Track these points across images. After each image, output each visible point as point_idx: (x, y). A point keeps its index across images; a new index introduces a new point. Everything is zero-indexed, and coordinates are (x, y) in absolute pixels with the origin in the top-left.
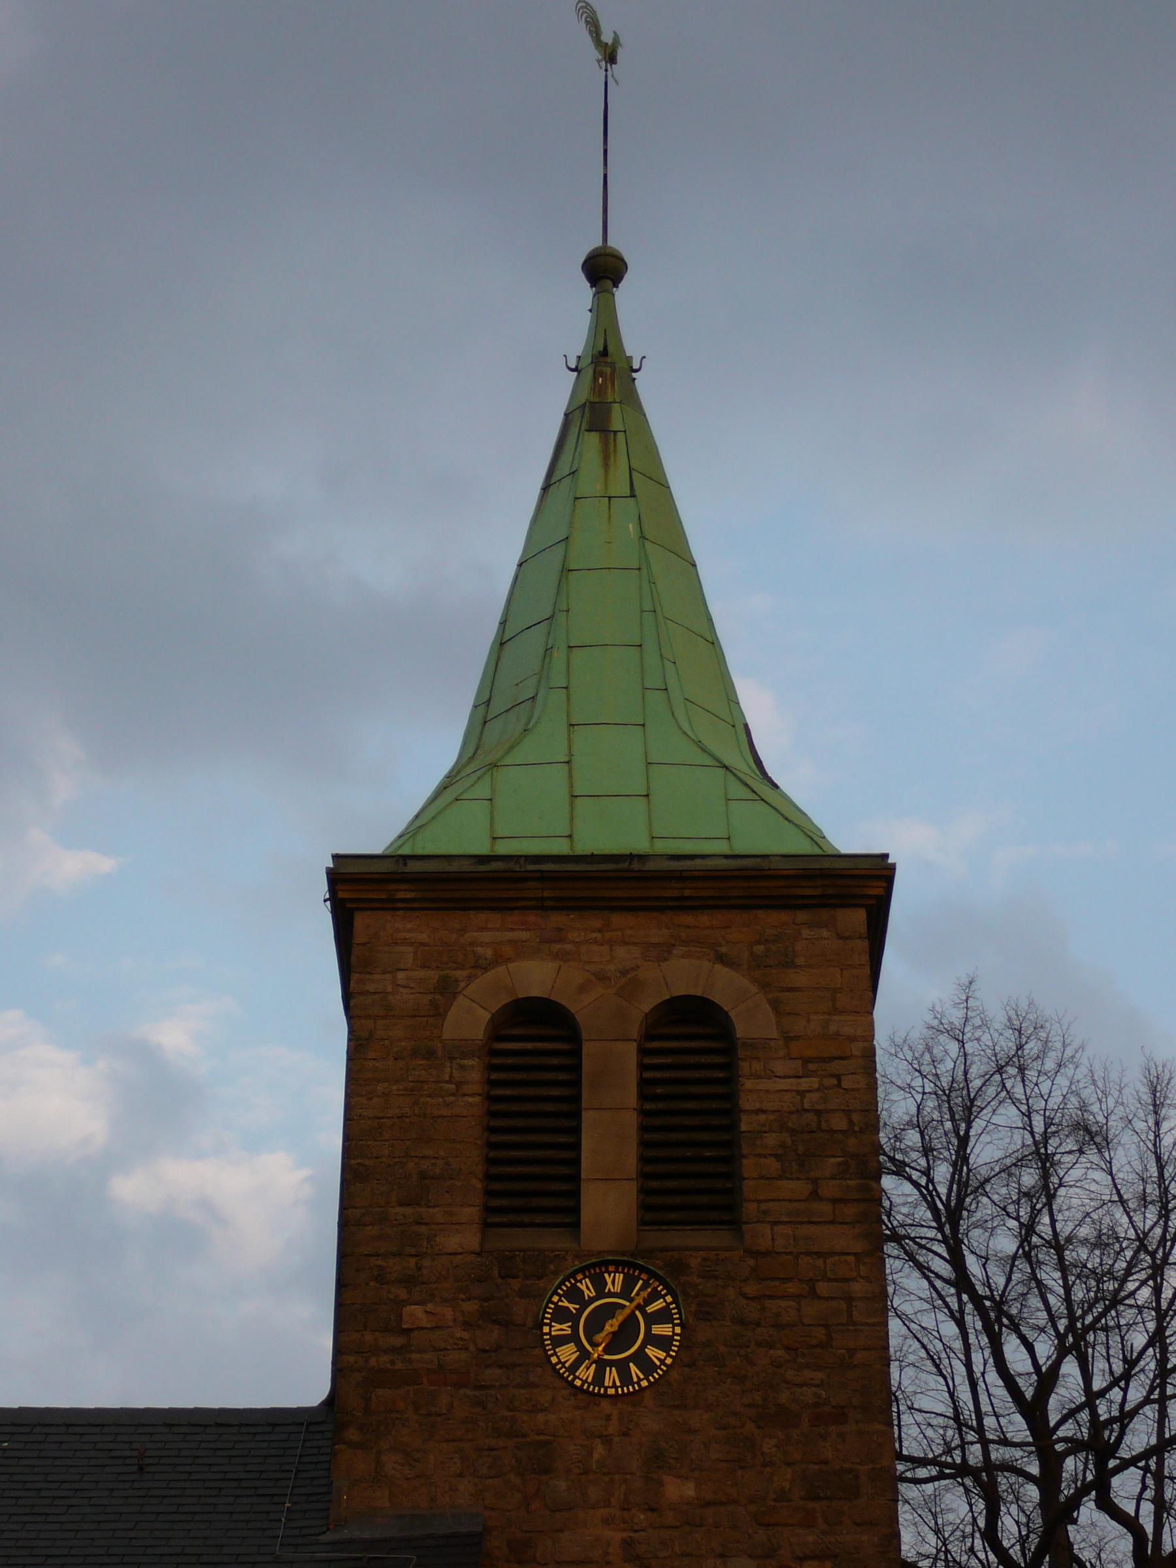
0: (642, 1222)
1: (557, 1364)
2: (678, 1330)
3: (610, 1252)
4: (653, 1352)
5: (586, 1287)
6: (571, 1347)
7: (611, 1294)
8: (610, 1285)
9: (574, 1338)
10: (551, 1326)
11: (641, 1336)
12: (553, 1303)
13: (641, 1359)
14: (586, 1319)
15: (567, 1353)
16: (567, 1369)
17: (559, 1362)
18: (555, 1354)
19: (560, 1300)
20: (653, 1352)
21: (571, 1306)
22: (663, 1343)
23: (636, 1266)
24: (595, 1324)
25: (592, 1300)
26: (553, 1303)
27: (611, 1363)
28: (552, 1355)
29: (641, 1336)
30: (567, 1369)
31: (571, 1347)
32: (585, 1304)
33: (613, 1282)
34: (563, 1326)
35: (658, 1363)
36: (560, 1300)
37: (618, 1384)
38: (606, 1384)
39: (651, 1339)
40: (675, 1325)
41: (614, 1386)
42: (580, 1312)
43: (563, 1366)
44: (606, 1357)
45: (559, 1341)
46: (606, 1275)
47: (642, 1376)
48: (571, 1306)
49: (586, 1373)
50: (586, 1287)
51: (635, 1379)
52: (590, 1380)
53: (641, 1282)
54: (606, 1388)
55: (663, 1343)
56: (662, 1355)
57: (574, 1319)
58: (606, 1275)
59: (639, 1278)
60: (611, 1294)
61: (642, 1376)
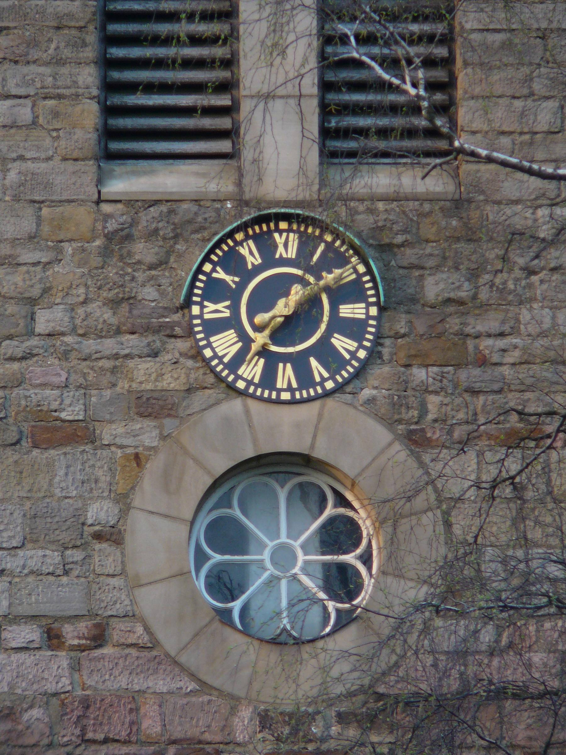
0: (328, 156)
1: (212, 358)
2: (374, 311)
3: (286, 204)
4: (342, 343)
5: (250, 254)
6: (230, 335)
7: (284, 262)
8: (281, 249)
9: (233, 322)
10: (202, 307)
11: (326, 319)
12: (204, 273)
13: (324, 352)
14: (293, 345)
15: (225, 344)
16: (226, 366)
17: (215, 356)
18: (209, 345)
19: (324, 380)
20: (342, 343)
21: (228, 278)
22: (354, 328)
23: (313, 222)
24: (264, 299)
25: (258, 270)
26: (204, 273)
27: (285, 358)
28: (205, 347)
29: (326, 319)
30: (226, 366)
31: (230, 335)
32: (247, 275)
33: (286, 245)
34: (220, 306)
35: (347, 356)
36: (324, 380)
37: (295, 385)
38: (279, 385)
39: (340, 325)
40: (369, 305)
41: (290, 389)
42: (242, 286)
43: (221, 362)
44: (274, 348)
45: (214, 327)
46: (276, 235)
47: (326, 375)
48: (228, 278)
49: (253, 370)
50: (250, 254)
51: (318, 379)
52: (256, 380)
53: (322, 247)
54: (279, 391)
55: (354, 328)
56: (352, 345)
57: (234, 296)
58: (276, 235)
59: (321, 238)
60: (284, 262)
61: (326, 375)
